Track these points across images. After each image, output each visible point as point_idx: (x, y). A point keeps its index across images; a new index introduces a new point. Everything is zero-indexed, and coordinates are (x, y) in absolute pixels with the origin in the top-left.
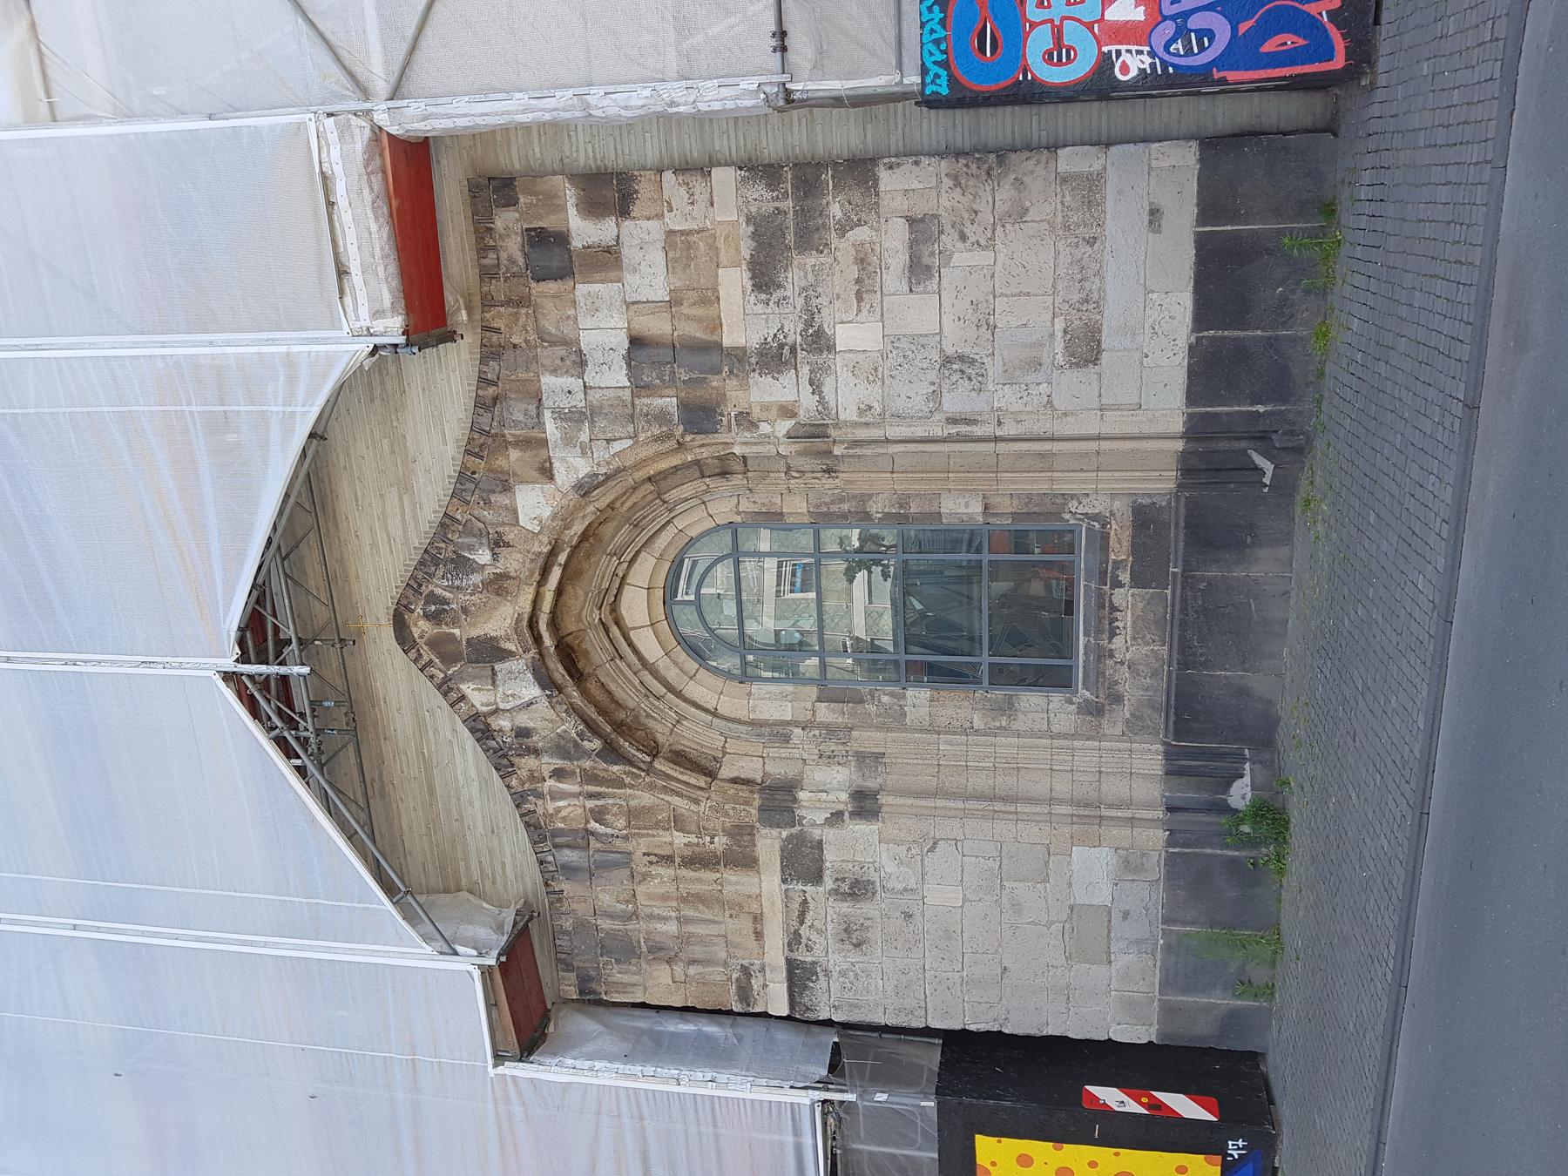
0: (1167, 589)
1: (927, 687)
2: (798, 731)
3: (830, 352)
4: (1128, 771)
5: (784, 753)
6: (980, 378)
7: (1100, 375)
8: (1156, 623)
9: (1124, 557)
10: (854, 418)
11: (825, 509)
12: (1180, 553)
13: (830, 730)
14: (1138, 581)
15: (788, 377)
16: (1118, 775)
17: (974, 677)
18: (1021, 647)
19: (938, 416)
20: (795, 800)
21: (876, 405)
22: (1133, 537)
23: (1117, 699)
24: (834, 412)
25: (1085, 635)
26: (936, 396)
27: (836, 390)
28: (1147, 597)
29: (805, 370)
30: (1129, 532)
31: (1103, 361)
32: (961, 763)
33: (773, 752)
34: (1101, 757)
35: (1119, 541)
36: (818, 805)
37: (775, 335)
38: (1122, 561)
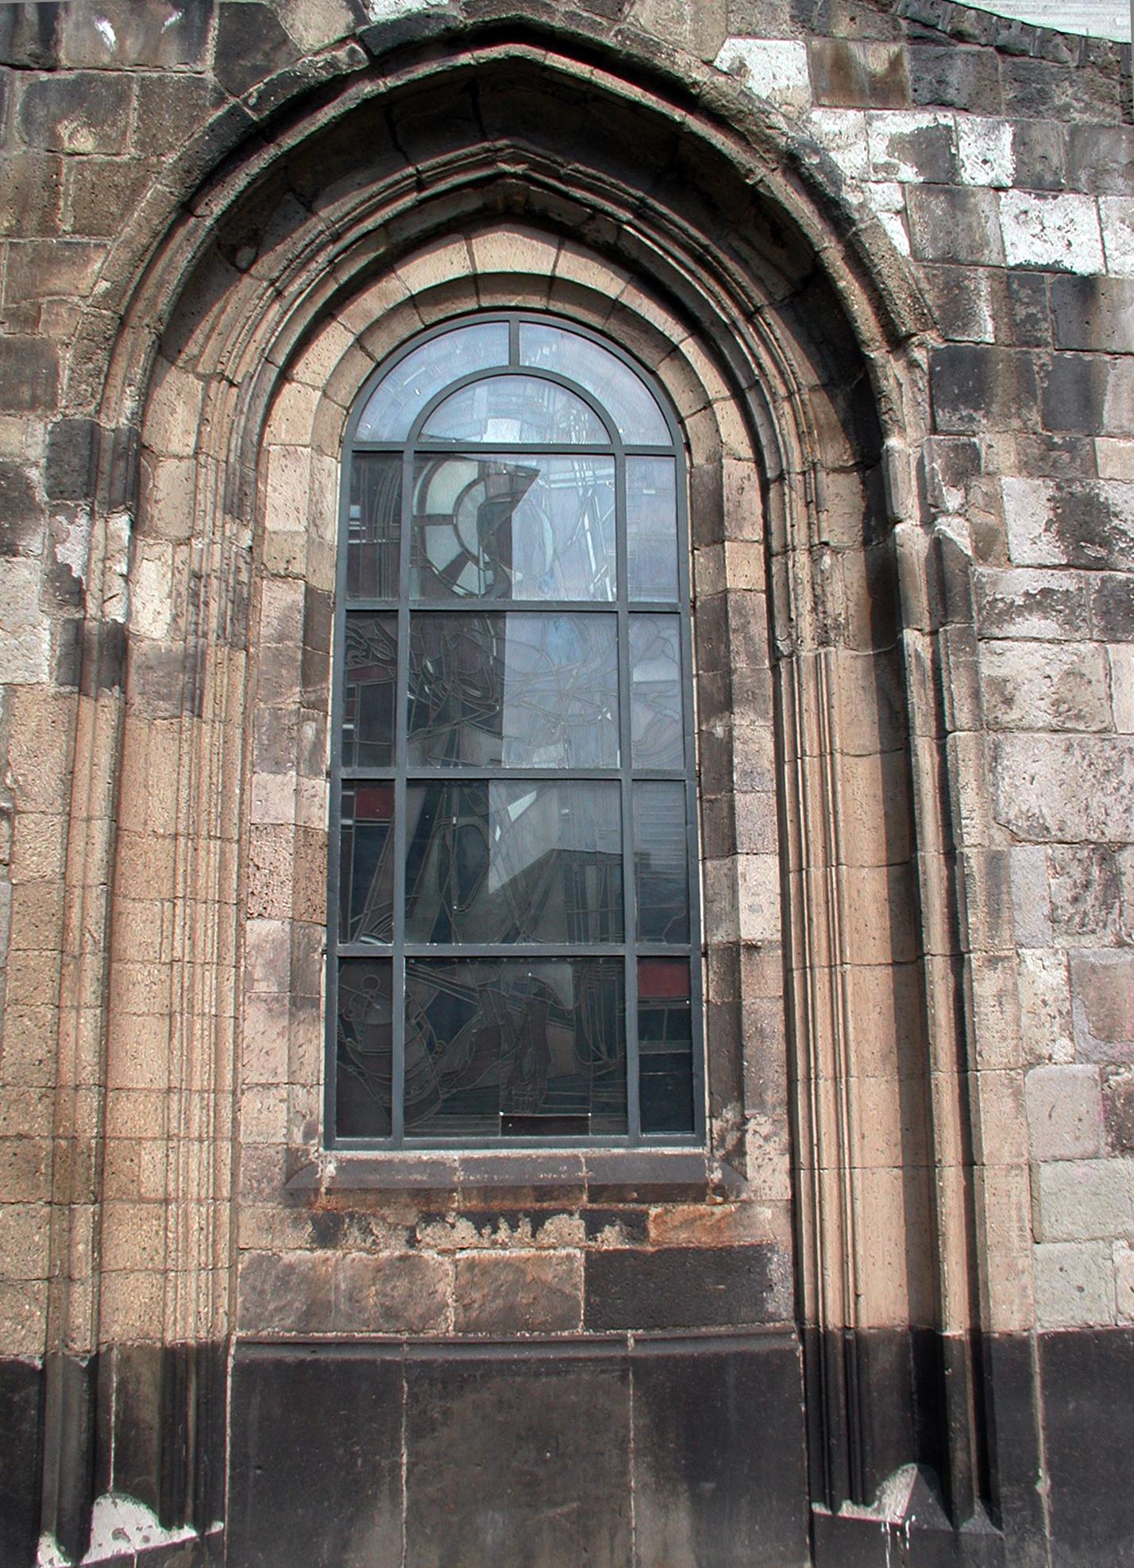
0: (587, 1327)
1: (331, 824)
2: (246, 539)
3: (1104, 630)
4: (170, 1264)
5: (206, 499)
6: (1077, 919)
7: (1095, 1156)
8: (511, 1308)
9: (653, 1233)
10: (985, 670)
11: (734, 623)
12: (678, 1350)
13: (243, 606)
14: (599, 1266)
15: (1050, 550)
16: (158, 1242)
17: (355, 925)
18: (428, 1026)
19: (1000, 837)
20: (112, 506)
21: (1014, 715)
22: (698, 1251)
23: (327, 1234)
24: (996, 632)
25: (465, 1162)
26: (1039, 833)
27: (1035, 639)
28: (568, 1289)
29: (1065, 582)
30: (707, 1240)
31: (1120, 1160)
32: (180, 887)
33: (208, 477)
34: (199, 1202)
35: (688, 1223)
36: (97, 554)
37: (1124, 533)
38: (645, 1230)
